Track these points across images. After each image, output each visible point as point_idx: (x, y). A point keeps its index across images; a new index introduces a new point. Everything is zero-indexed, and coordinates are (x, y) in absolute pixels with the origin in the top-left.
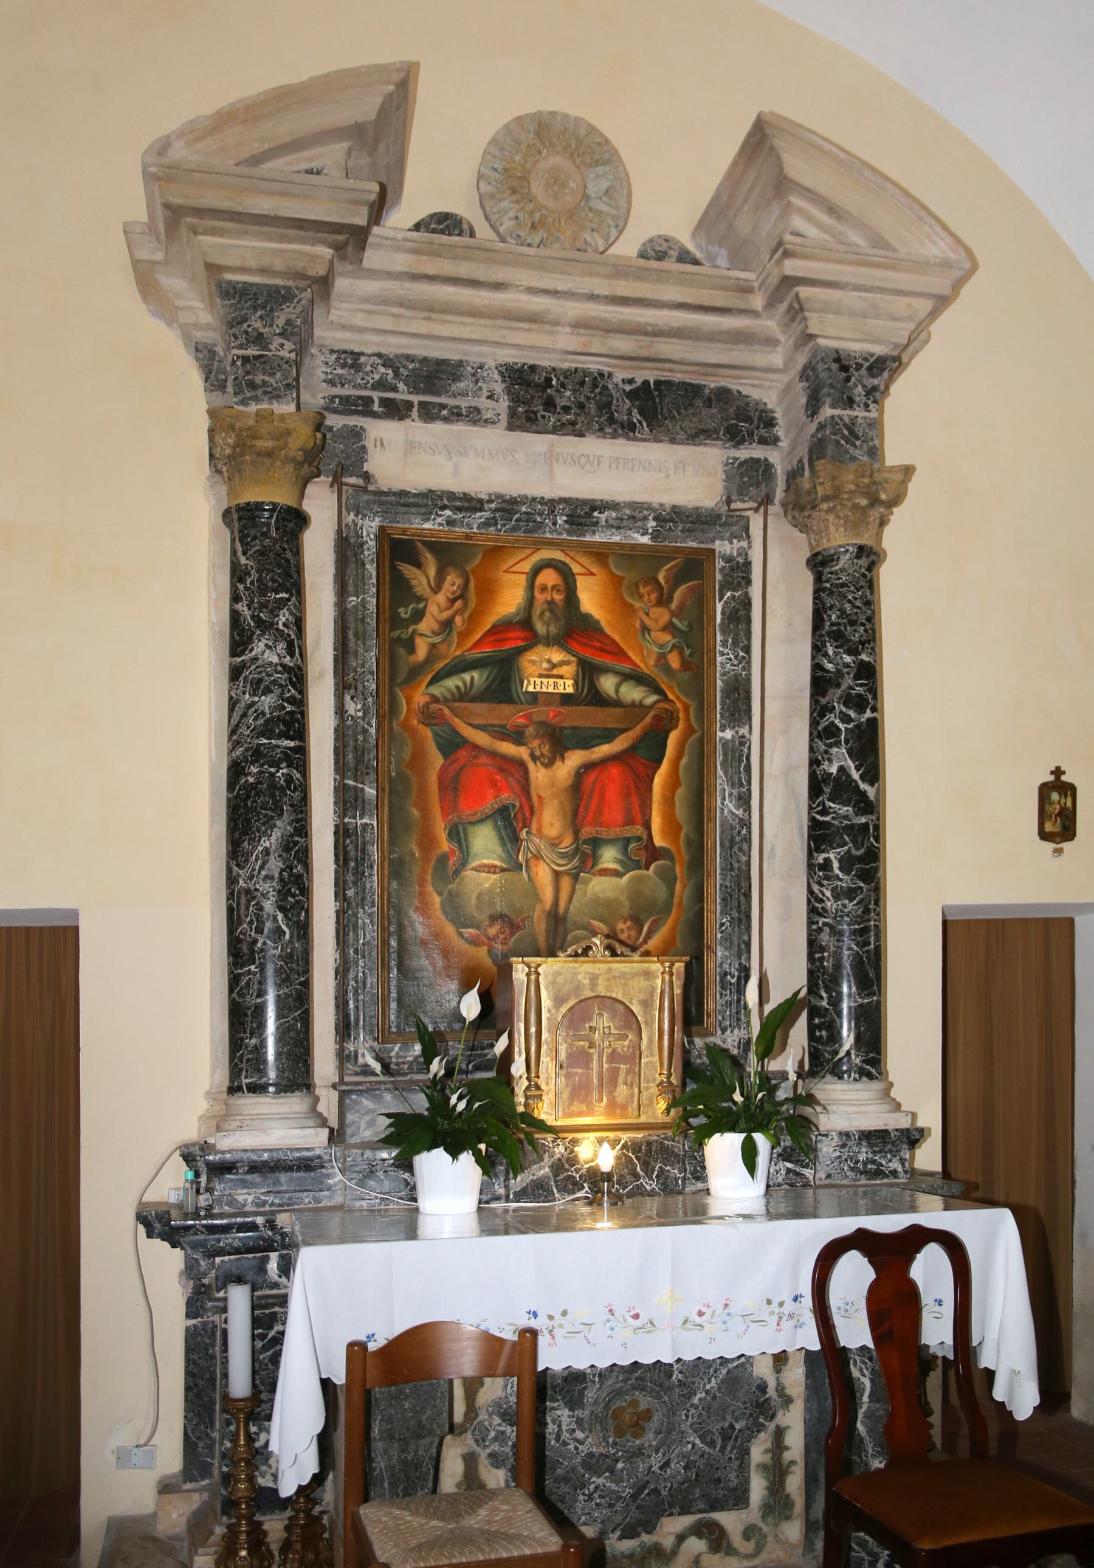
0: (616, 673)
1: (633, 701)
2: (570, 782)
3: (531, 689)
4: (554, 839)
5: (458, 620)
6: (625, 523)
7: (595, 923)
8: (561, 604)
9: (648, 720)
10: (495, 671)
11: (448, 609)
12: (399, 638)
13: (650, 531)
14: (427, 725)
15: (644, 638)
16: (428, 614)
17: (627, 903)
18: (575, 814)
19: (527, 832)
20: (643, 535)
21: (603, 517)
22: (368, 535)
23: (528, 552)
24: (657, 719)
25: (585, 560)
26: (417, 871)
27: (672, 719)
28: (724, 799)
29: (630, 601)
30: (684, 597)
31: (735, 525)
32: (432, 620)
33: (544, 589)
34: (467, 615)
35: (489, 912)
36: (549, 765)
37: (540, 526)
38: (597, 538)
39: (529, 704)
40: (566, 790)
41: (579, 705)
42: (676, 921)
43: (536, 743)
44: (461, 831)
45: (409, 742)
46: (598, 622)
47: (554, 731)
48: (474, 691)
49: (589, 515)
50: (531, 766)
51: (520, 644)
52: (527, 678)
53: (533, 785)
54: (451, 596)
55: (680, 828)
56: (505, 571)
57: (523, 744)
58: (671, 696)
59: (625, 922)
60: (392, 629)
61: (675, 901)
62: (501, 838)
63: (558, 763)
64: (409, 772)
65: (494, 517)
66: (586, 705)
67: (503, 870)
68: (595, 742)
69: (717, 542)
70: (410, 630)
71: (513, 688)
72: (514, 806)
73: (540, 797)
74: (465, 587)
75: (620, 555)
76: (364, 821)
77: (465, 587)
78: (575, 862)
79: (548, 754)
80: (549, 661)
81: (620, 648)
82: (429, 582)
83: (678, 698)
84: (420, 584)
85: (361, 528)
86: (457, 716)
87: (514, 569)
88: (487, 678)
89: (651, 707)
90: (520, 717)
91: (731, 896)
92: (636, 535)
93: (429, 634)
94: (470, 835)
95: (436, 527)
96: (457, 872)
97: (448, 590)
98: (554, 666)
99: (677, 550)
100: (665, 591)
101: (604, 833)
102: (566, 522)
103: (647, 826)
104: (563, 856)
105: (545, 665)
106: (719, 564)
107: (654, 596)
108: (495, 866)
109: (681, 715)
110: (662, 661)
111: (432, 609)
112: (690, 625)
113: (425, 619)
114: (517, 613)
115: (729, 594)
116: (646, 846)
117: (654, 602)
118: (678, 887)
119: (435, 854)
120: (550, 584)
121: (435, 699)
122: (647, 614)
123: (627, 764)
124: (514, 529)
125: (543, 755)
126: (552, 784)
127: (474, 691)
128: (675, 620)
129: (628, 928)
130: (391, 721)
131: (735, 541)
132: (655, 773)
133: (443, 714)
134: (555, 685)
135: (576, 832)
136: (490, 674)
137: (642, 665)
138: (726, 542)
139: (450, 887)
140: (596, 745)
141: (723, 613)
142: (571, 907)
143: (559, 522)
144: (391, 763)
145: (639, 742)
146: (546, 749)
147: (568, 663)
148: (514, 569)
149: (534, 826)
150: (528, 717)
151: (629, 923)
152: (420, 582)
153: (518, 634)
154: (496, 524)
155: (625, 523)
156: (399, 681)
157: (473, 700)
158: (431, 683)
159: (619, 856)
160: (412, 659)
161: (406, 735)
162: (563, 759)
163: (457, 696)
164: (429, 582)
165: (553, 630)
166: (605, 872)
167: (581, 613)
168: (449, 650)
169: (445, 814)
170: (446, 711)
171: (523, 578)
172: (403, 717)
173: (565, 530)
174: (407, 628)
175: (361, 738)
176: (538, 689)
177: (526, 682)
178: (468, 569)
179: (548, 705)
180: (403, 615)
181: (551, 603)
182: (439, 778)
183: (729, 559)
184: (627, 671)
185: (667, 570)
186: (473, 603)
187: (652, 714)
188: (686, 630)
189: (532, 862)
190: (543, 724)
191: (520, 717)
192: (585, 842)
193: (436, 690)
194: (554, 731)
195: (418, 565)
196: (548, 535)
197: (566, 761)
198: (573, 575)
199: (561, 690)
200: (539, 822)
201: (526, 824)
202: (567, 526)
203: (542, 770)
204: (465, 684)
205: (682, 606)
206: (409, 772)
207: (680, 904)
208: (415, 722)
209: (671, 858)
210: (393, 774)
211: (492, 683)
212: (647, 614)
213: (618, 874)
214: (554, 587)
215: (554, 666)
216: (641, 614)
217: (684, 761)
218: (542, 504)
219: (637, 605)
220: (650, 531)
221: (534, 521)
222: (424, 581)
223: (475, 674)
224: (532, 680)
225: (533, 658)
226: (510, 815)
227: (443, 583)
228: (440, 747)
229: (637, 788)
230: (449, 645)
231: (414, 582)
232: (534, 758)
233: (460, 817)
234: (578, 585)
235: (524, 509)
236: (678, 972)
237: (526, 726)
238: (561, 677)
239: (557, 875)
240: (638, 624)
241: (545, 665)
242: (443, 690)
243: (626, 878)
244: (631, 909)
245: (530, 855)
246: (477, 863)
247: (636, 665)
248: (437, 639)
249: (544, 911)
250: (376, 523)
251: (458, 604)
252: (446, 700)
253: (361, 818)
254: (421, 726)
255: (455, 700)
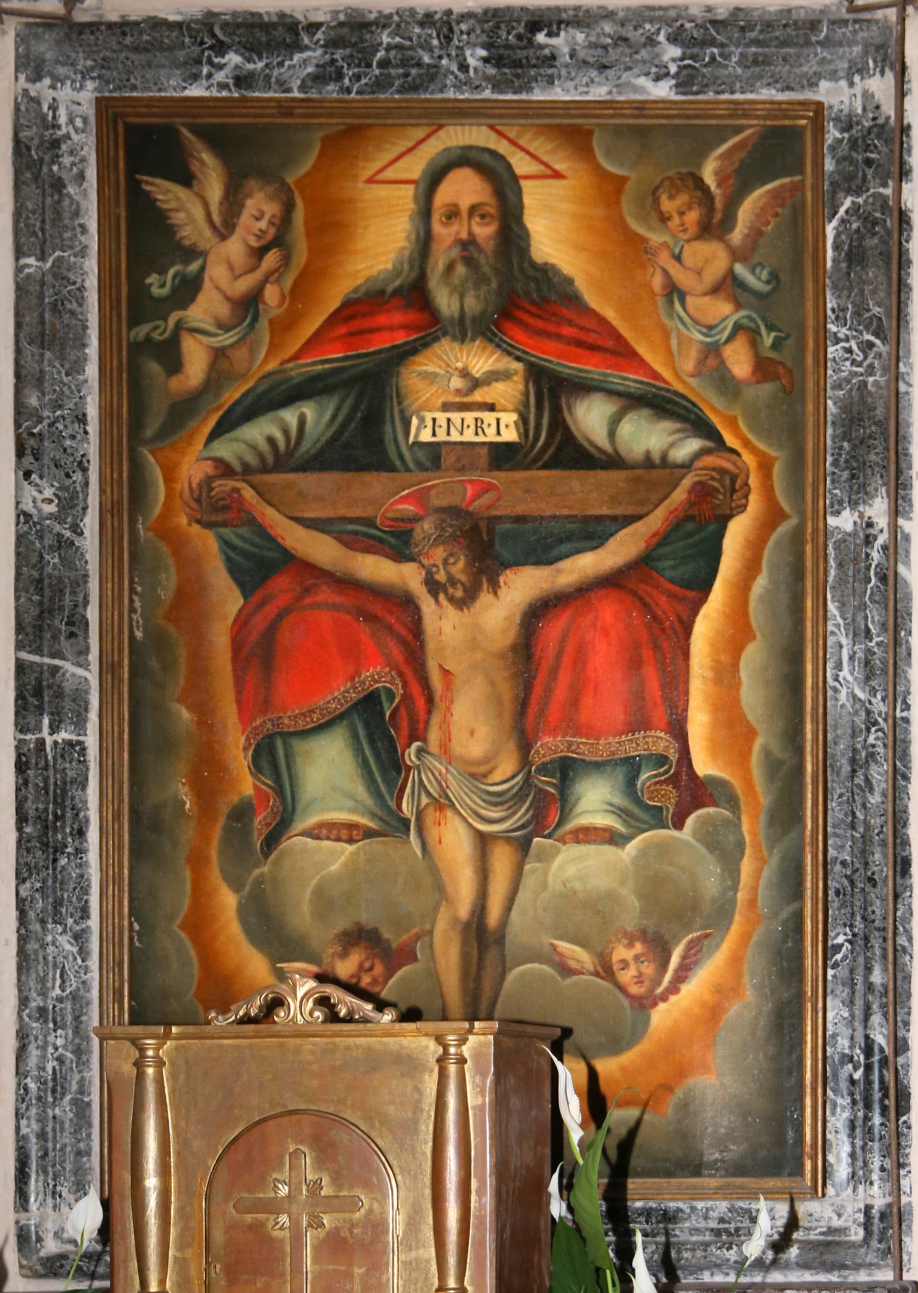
0: (611, 393)
1: (648, 455)
2: (510, 637)
3: (426, 436)
4: (478, 763)
5: (271, 294)
6: (613, 54)
7: (563, 946)
8: (490, 247)
9: (679, 495)
10: (349, 402)
11: (252, 270)
12: (148, 339)
13: (673, 69)
14: (208, 525)
15: (671, 312)
16: (207, 284)
17: (633, 903)
18: (523, 705)
19: (420, 751)
20: (658, 78)
21: (561, 42)
22: (71, 121)
23: (420, 133)
24: (701, 491)
25: (540, 146)
26: (188, 833)
27: (733, 491)
28: (839, 666)
29: (641, 231)
30: (761, 215)
31: (851, 43)
32: (217, 297)
33: (452, 214)
34: (288, 282)
35: (342, 923)
36: (465, 602)
37: (432, 74)
38: (559, 93)
39: (422, 467)
40: (502, 656)
41: (528, 467)
42: (745, 938)
43: (439, 554)
44: (281, 752)
45: (171, 562)
46: (570, 281)
47: (475, 528)
48: (306, 445)
49: (526, 40)
50: (427, 605)
51: (401, 338)
52: (417, 412)
53: (431, 646)
54: (255, 243)
55: (751, 734)
56: (370, 181)
57: (412, 559)
58: (730, 440)
59: (630, 945)
60: (134, 322)
61: (741, 896)
62: (364, 764)
63: (485, 597)
64: (171, 629)
65: (333, 61)
66: (545, 467)
67: (369, 834)
68: (565, 548)
69: (824, 85)
70: (172, 321)
71: (388, 436)
72: (391, 695)
73: (446, 673)
74: (285, 221)
75: (618, 131)
76: (63, 735)
77: (285, 221)
78: (521, 815)
79: (463, 578)
80: (465, 373)
81: (619, 338)
82: (208, 215)
83: (746, 443)
84: (191, 220)
85: (54, 108)
86: (270, 503)
87: (388, 174)
88: (334, 417)
89: (687, 466)
90: (403, 500)
91: (852, 883)
92: (642, 81)
93: (212, 329)
94: (299, 760)
95: (215, 93)
96: (272, 841)
97: (248, 230)
98: (476, 384)
99: (741, 110)
100: (719, 204)
101: (583, 748)
102: (486, 60)
103: (680, 733)
104: (496, 800)
105: (457, 382)
106: (833, 133)
107: (693, 216)
108: (352, 826)
109: (753, 481)
110: (711, 362)
111: (217, 273)
112: (774, 277)
113: (201, 298)
114: (397, 272)
115: (848, 203)
116: (677, 774)
117: (693, 230)
118: (746, 866)
119: (224, 807)
120: (465, 203)
121: (225, 469)
122: (678, 258)
123: (634, 593)
124: (380, 85)
125: (452, 581)
126: (473, 643)
127: (306, 445)
128: (739, 269)
129: (637, 958)
130: (133, 522)
131: (857, 78)
132: (695, 612)
133: (241, 500)
134: (479, 426)
135: (525, 746)
136: (337, 410)
137: (666, 374)
138: (843, 83)
139: (257, 872)
140: (567, 556)
141: (837, 247)
142: (514, 915)
143: (472, 62)
144: (132, 610)
145: (659, 545)
146: (459, 568)
147: (505, 375)
148: (388, 174)
149: (434, 736)
150: (420, 497)
151: (639, 948)
152: (188, 212)
153: (398, 317)
154: (340, 76)
155: (613, 54)
156: (149, 433)
157: (305, 467)
158: (215, 434)
159: (618, 800)
160: (176, 384)
161: (165, 549)
162: (495, 587)
163: (270, 460)
164: (208, 215)
165: (472, 304)
166: (586, 835)
167: (533, 264)
168: (251, 362)
169: (245, 716)
170: (248, 493)
171: (406, 196)
172: (157, 510)
173: (487, 78)
174: (165, 320)
175: (53, 559)
176: (441, 437)
177: (415, 421)
178: (290, 180)
179: (462, 470)
180: (156, 291)
181: (468, 244)
182: (234, 640)
183: (848, 123)
184: (633, 387)
185: (722, 157)
186: (301, 257)
187: (687, 482)
188: (767, 288)
189: (431, 816)
190: (453, 511)
191: (403, 500)
192: (544, 769)
193: (225, 449)
194: (475, 528)
195: (186, 179)
196: (451, 94)
197: (503, 592)
198: (515, 179)
199: (491, 436)
200: (445, 725)
201: (417, 734)
202: (491, 71)
203: (451, 612)
204: (286, 432)
205: (756, 234)
206: (171, 629)
207: (752, 903)
208: (184, 520)
209: (733, 803)
210: (139, 634)
211: (343, 427)
212: (678, 258)
213: (613, 838)
214: (473, 209)
215: (476, 384)
216: (664, 259)
217: (760, 584)
218: (422, 24)
219: (656, 238)
220: (673, 69)
221: (419, 64)
222: (198, 212)
223: (309, 410)
224: (429, 416)
225: (431, 368)
226: (382, 713)
227: (239, 215)
228: (234, 570)
229: (656, 647)
230: (252, 352)
231: (178, 218)
232: (433, 587)
233: (277, 722)
234: (527, 200)
235: (385, 39)
236: (478, 1055)
237: (416, 519)
238: (492, 408)
239: (483, 842)
240: (657, 282)
241: (457, 382)
242: (240, 448)
243: (632, 847)
244: (644, 913)
245: (425, 800)
246: (312, 820)
247: (656, 376)
248: (226, 339)
249: (456, 920)
250: (88, 95)
251: (271, 259)
252: (247, 469)
253: (53, 730)
254: (196, 528)
255: (265, 469)
